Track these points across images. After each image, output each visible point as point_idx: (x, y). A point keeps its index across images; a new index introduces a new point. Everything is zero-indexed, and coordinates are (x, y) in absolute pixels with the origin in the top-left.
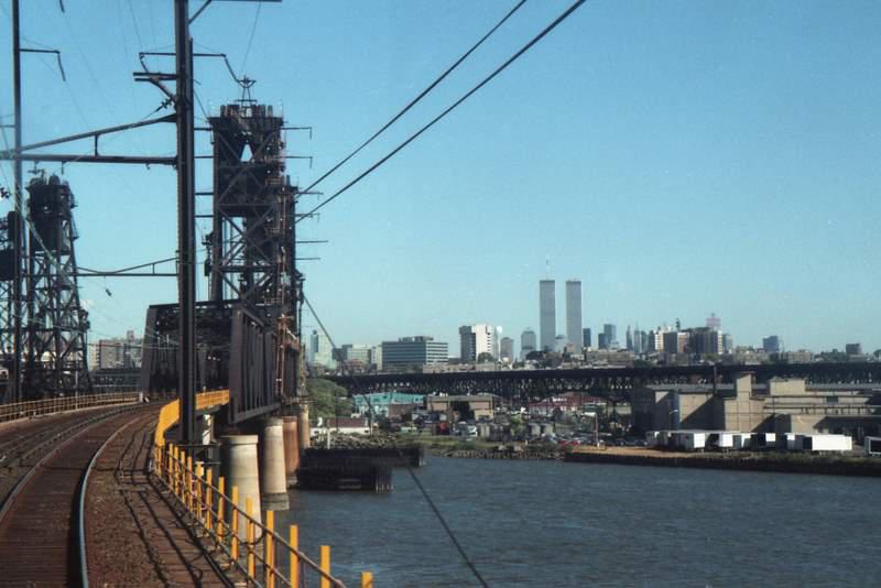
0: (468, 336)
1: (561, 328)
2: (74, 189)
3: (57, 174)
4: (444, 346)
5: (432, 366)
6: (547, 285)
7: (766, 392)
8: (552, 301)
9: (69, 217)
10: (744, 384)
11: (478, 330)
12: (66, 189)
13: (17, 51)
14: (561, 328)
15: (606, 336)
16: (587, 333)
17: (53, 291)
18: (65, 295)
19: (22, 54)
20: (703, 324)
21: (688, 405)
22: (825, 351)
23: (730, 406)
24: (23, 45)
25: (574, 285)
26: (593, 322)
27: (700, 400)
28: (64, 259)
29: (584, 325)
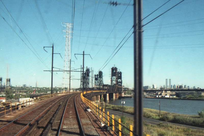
0: (153, 86)
1: (168, 85)
2: (103, 72)
3: (90, 69)
4: (150, 87)
5: (149, 89)
6: (167, 80)
7: (166, 92)
8: (167, 81)
9: (102, 75)
10: (164, 91)
11: (155, 85)
12: (102, 72)
13: (53, 54)
14: (168, 85)
15: (174, 86)
16: (172, 86)
17: (101, 81)
18: (102, 82)
19: (84, 55)
20: (181, 85)
21: (159, 93)
22: (28, 85)
23: (162, 93)
24: (54, 53)
25: (170, 80)
26: (172, 84)
27: (160, 93)
28: (102, 79)
29: (171, 85)
